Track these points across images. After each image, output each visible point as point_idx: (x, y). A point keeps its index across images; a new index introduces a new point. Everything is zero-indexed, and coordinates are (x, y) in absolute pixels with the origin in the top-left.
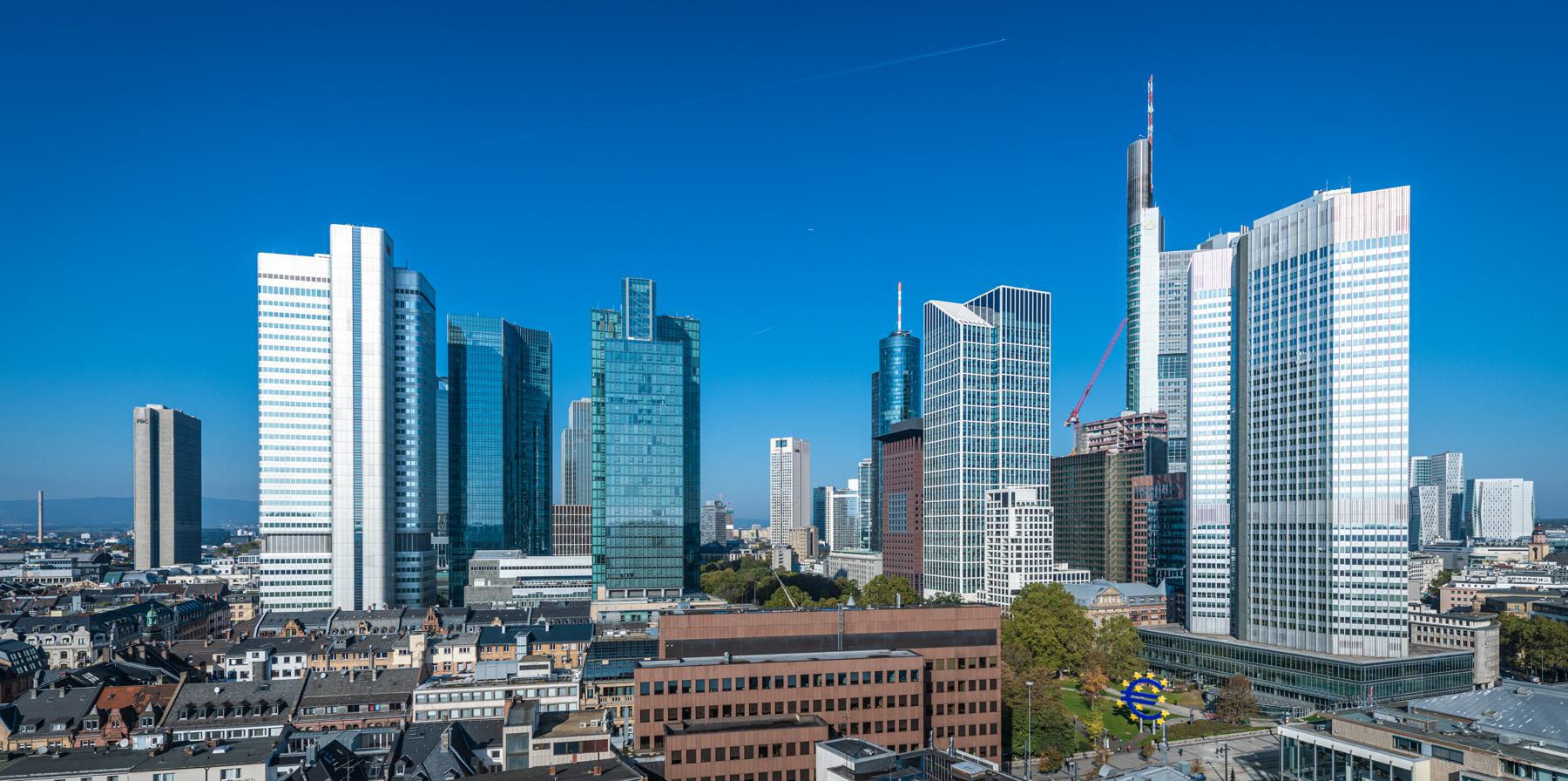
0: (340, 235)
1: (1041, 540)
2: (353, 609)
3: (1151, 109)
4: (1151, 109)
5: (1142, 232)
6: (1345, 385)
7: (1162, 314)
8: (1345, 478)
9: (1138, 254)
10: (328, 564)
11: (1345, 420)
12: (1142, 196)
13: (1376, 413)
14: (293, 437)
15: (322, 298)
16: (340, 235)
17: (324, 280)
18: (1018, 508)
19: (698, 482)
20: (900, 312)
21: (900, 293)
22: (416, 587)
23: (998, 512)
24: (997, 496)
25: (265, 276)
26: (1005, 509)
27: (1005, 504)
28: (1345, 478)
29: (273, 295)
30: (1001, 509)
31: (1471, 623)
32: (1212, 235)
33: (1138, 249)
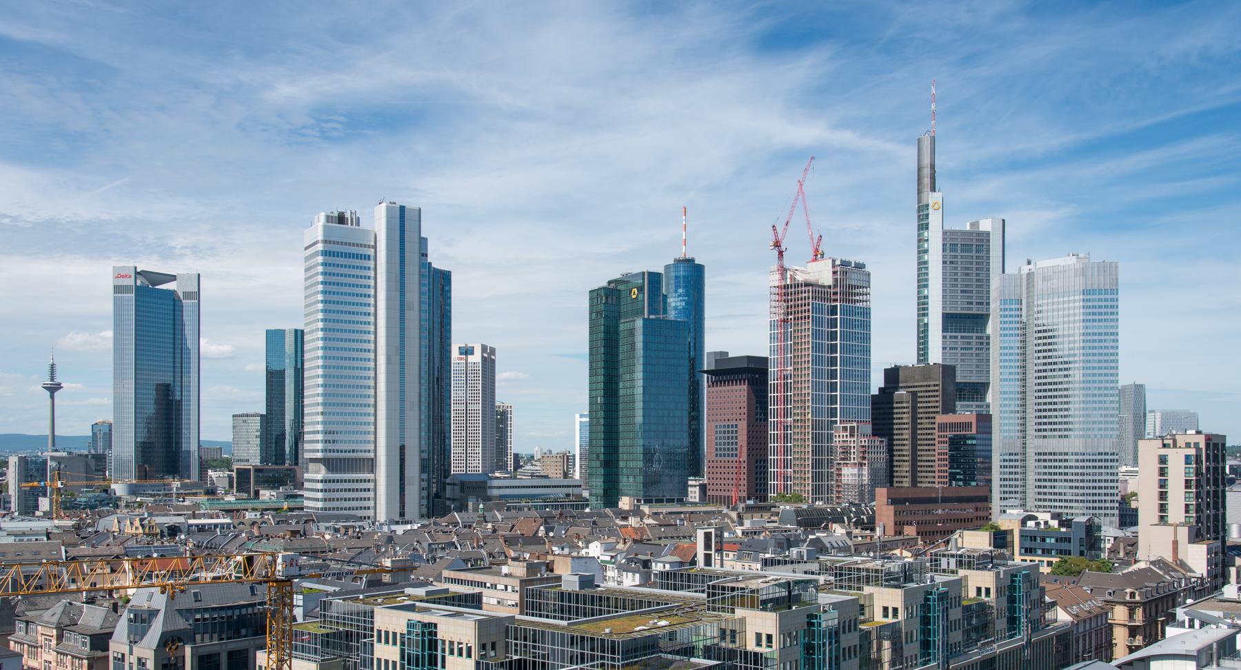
2: (377, 610)
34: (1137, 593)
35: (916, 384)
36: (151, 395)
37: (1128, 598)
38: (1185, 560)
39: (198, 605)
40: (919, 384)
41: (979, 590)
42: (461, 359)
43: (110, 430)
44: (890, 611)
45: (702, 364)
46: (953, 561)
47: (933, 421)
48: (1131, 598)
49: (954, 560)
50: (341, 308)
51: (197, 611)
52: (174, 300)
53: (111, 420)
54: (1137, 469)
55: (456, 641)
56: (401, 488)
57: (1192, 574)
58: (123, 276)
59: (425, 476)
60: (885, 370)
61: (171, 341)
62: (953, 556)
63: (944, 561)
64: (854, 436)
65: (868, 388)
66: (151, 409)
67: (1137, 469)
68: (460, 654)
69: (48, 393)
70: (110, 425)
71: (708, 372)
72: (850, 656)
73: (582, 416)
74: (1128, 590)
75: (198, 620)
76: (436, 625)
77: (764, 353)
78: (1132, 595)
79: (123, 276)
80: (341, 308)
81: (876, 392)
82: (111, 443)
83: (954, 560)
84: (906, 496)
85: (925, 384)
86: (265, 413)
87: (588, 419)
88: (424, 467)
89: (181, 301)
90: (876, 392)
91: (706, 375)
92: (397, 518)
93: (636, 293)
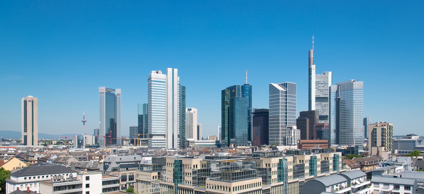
0: (170, 70)
1: (291, 134)
2: (174, 69)
3: (313, 43)
4: (313, 43)
5: (312, 70)
6: (355, 98)
7: (316, 85)
8: (355, 107)
9: (311, 75)
10: (165, 141)
11: (355, 111)
12: (312, 62)
13: (359, 113)
14: (160, 113)
15: (164, 83)
16: (170, 70)
17: (164, 79)
18: (294, 130)
19: (222, 120)
20: (247, 78)
21: (247, 73)
22: (152, 143)
23: (289, 131)
24: (289, 128)
25: (153, 78)
26: (291, 130)
27: (291, 129)
28: (355, 107)
29: (160, 83)
30: (290, 130)
31: (89, 150)
32: (325, 71)
33: (311, 73)
34: (368, 163)
35: (308, 116)
36: (109, 121)
37: (366, 164)
38: (381, 156)
39: (121, 161)
40: (309, 116)
41: (325, 158)
42: (188, 112)
43: (99, 131)
44: (301, 161)
45: (251, 111)
46: (318, 151)
47: (313, 125)
48: (366, 164)
49: (319, 151)
50: (157, 98)
51: (121, 162)
52: (115, 96)
53: (99, 128)
54: (368, 140)
55: (187, 164)
56: (173, 91)
57: (383, 159)
58: (102, 90)
59: (179, 139)
60: (300, 112)
61: (114, 100)
62: (318, 150)
63: (316, 151)
64: (292, 129)
65: (295, 117)
66: (109, 126)
67: (368, 140)
68: (188, 173)
69: (83, 123)
70: (99, 130)
71: (253, 113)
72: (290, 171)
73: (219, 126)
74: (366, 162)
75: (121, 165)
76: (182, 161)
77: (268, 108)
78: (367, 163)
79: (102, 90)
80: (157, 98)
81: (298, 118)
82: (99, 134)
83: (319, 151)
84: (306, 142)
85: (311, 116)
86: (138, 126)
87: (221, 127)
88: (179, 136)
89: (116, 96)
90: (298, 118)
91: (252, 114)
92: (172, 148)
93: (234, 91)
